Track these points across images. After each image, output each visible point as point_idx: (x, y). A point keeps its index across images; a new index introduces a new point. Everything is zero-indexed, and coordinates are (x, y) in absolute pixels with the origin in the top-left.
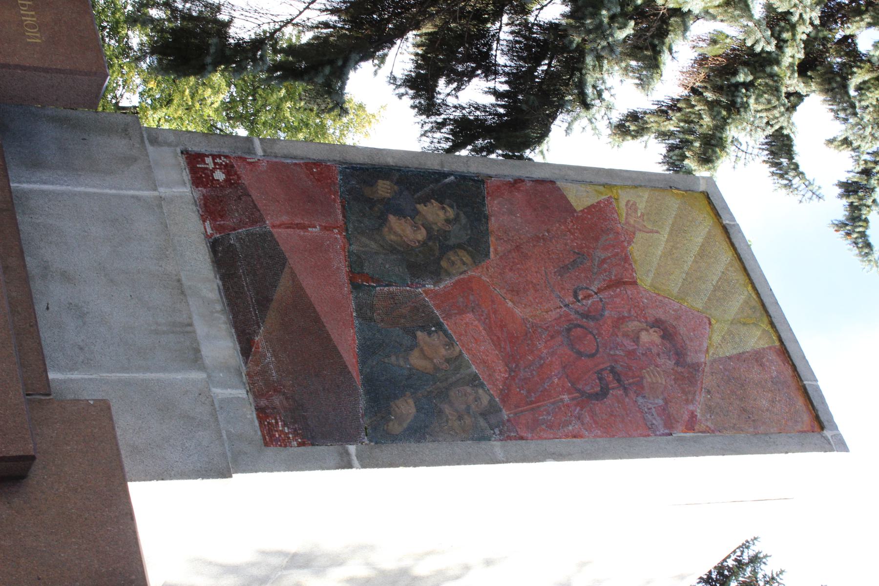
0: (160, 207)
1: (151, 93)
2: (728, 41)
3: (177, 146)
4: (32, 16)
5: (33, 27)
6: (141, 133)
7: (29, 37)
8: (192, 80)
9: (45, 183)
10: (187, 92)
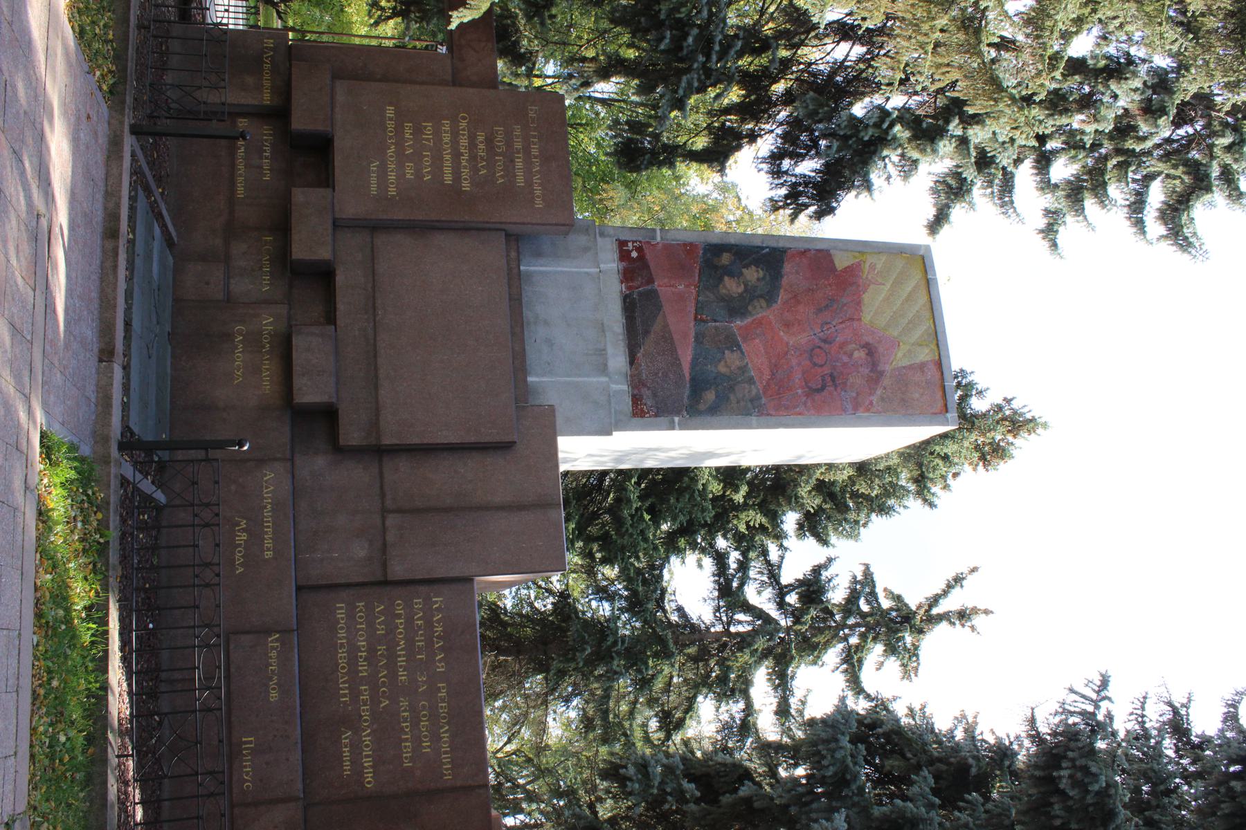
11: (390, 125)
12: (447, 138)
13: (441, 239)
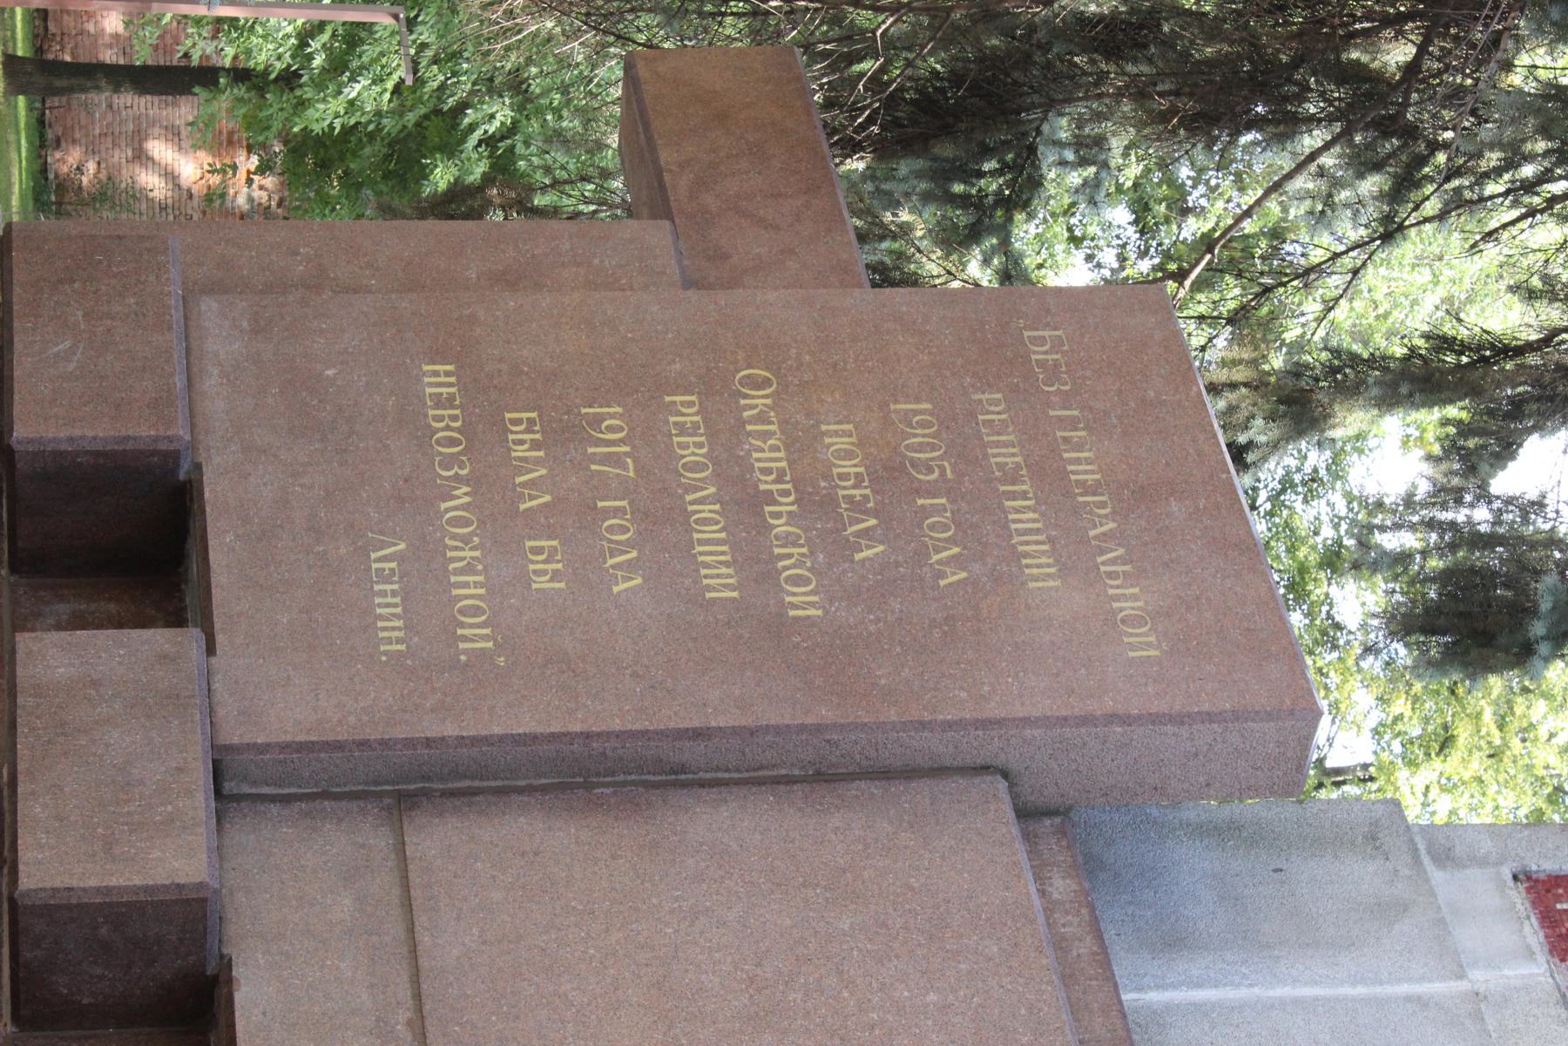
0: (1478, 1017)
1: (1399, 727)
2: (1432, 207)
3: (1499, 863)
4: (1135, 598)
5: (1137, 621)
6: (1412, 840)
7: (1132, 647)
8: (1496, 683)
9: (1199, 985)
10: (1488, 717)
11: (445, 423)
12: (692, 449)
13: (714, 824)
